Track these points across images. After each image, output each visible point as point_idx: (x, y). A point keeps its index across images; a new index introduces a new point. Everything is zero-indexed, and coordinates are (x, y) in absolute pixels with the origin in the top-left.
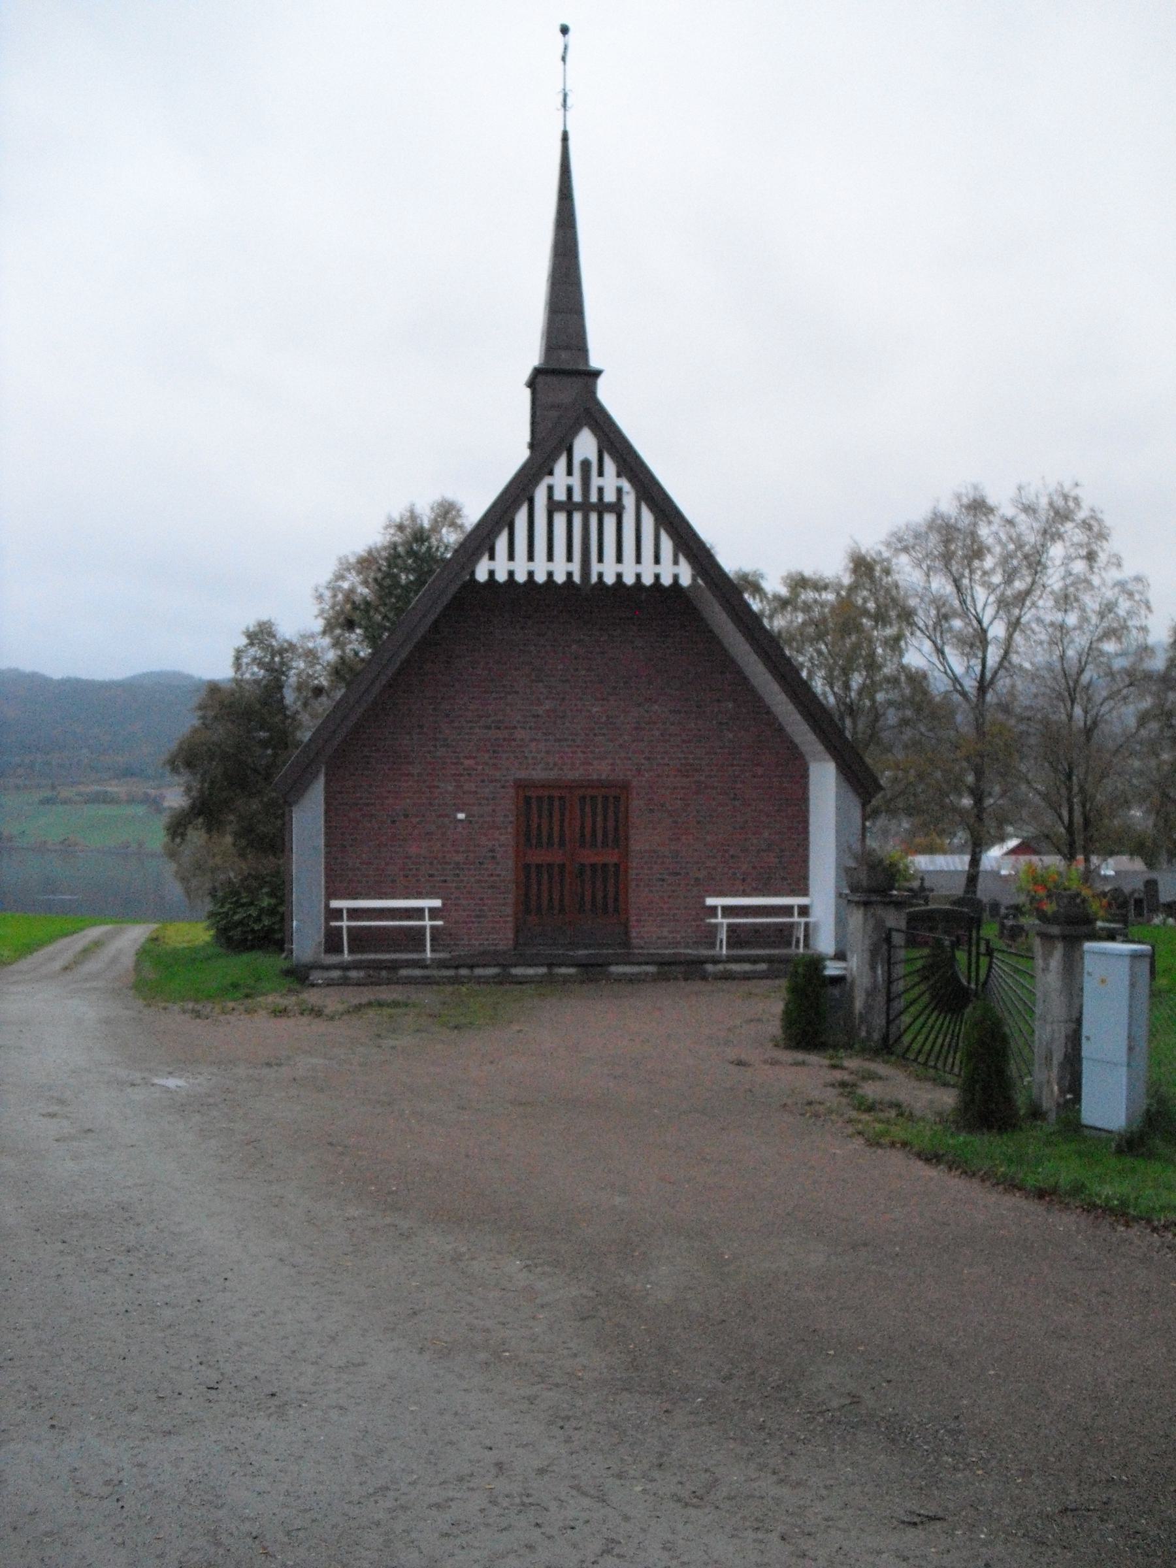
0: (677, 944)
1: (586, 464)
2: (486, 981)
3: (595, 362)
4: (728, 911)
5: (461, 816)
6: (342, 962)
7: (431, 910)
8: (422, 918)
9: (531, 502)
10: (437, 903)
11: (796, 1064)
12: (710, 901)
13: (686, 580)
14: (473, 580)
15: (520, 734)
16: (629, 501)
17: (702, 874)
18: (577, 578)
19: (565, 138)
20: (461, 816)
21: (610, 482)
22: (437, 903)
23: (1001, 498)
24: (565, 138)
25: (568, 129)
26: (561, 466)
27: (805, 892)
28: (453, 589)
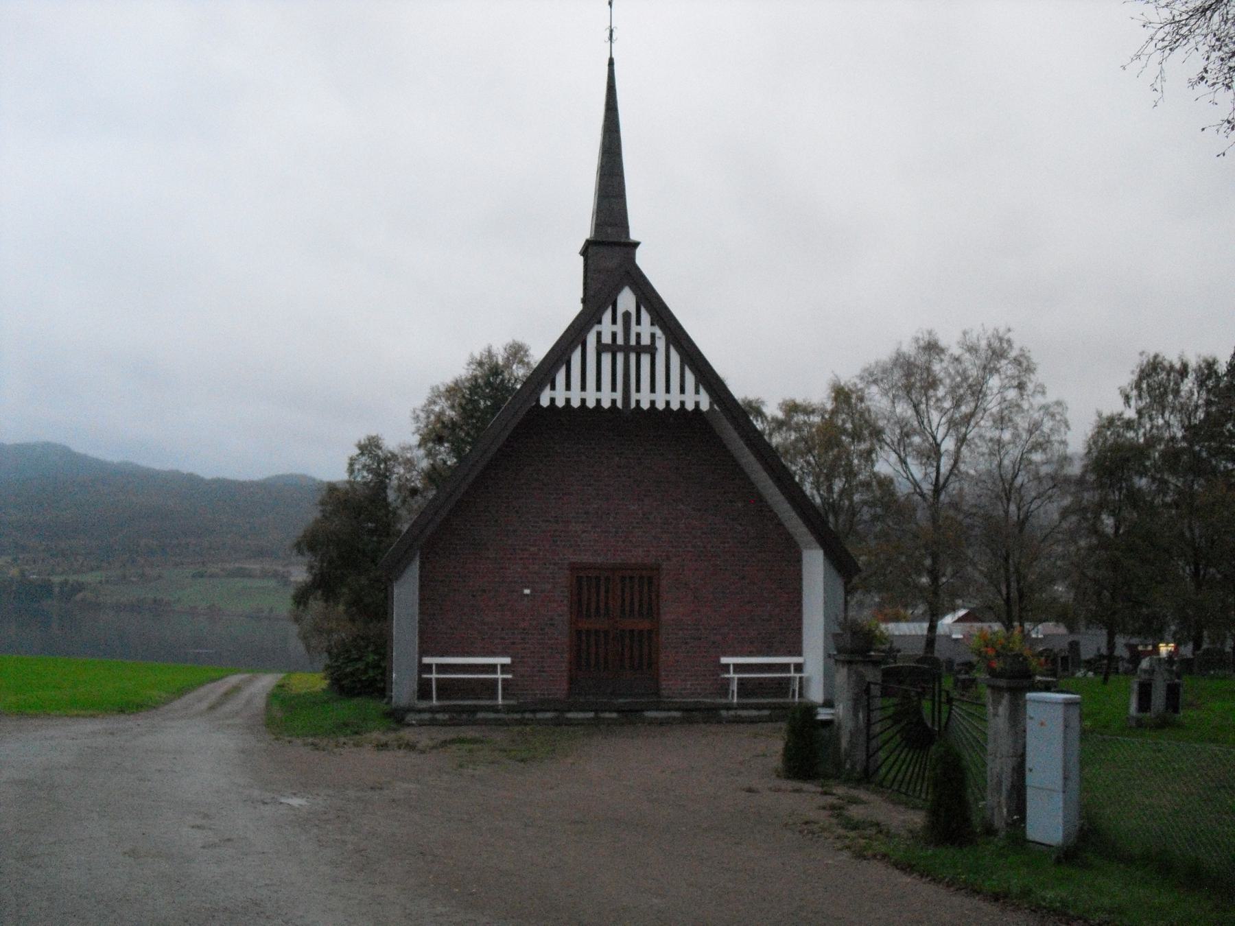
1: (627, 315)
4: (739, 668)
5: (527, 591)
7: (503, 666)
8: (495, 672)
10: (507, 660)
12: (724, 660)
14: (538, 405)
16: (661, 344)
18: (619, 404)
20: (527, 591)
21: (646, 329)
23: (950, 340)
26: (607, 316)
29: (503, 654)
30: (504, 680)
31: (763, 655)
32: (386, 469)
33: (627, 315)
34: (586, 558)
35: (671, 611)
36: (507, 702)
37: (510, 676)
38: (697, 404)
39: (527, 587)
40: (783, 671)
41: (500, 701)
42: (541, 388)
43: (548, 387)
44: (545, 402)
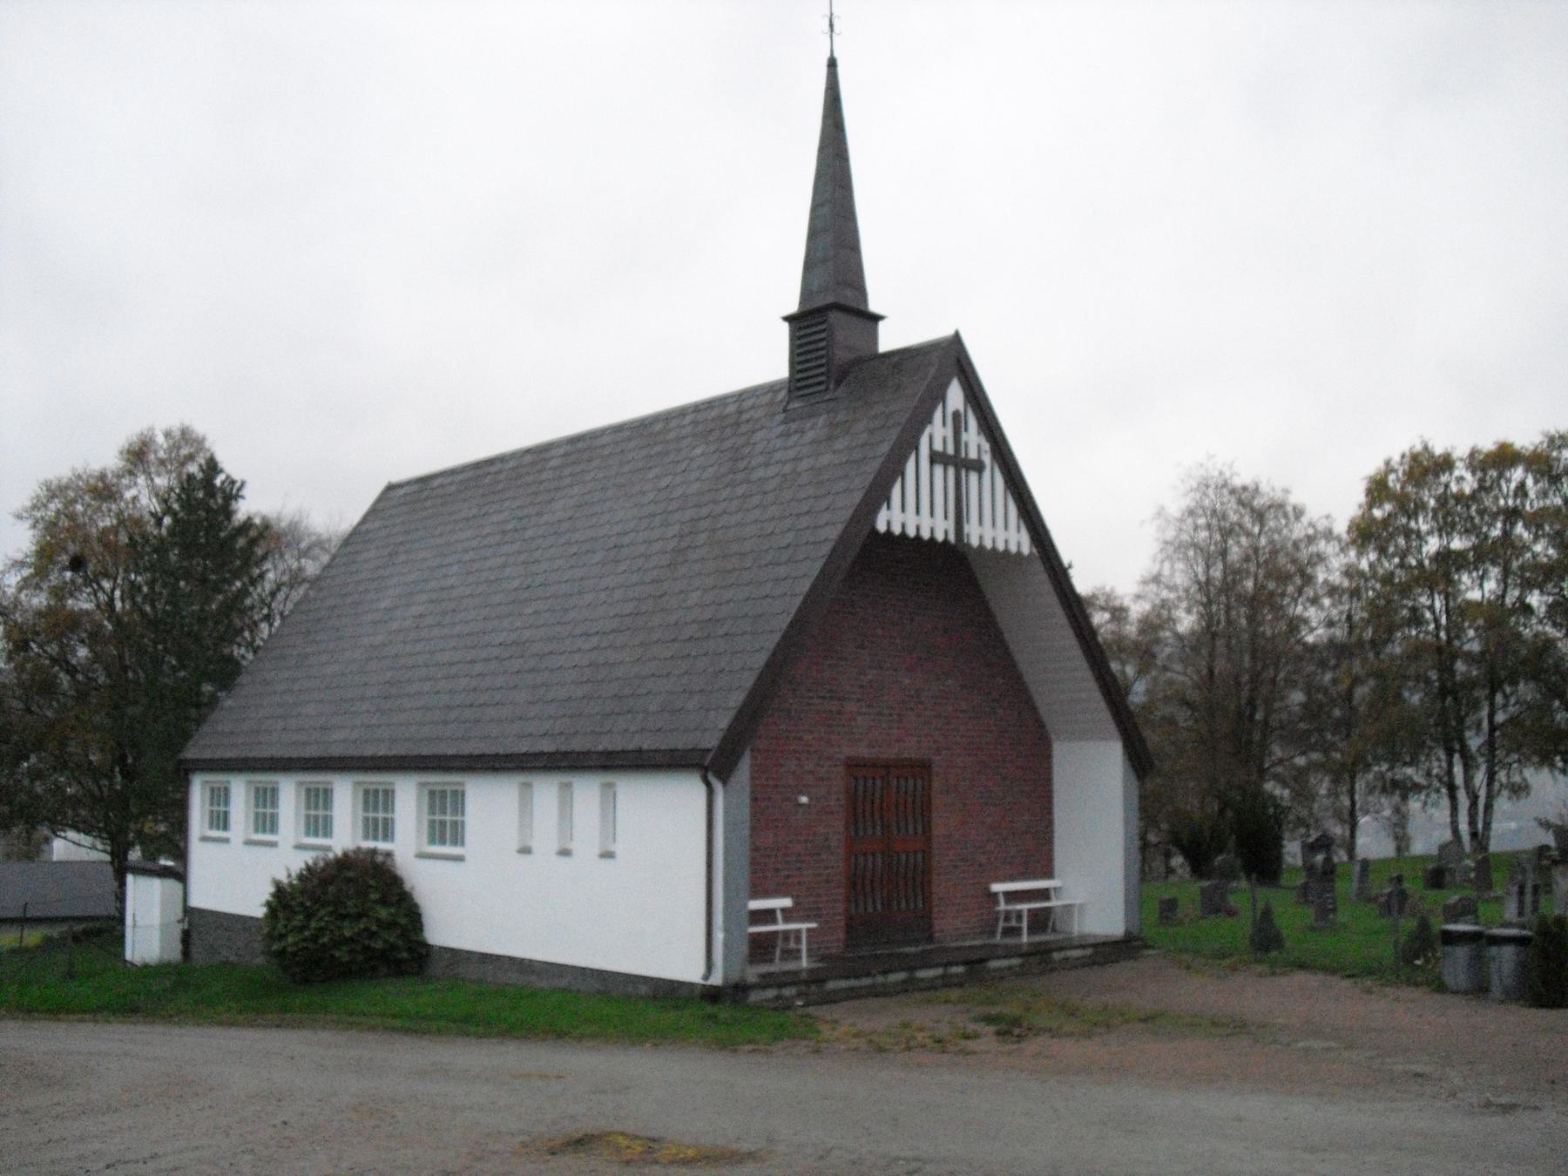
0: (964, 936)
1: (956, 415)
2: (931, 985)
3: (874, 306)
4: (1012, 896)
5: (804, 799)
6: (796, 973)
7: (783, 910)
8: (774, 921)
9: (917, 449)
10: (787, 902)
11: (1010, 1053)
12: (997, 887)
13: (1026, 550)
14: (874, 532)
15: (850, 707)
16: (987, 459)
17: (983, 859)
18: (952, 538)
19: (832, 64)
20: (804, 799)
21: (974, 442)
22: (787, 902)
23: (1264, 488)
24: (832, 64)
25: (836, 55)
26: (938, 415)
27: (1049, 874)
28: (859, 541)
29: (785, 895)
30: (809, 930)
31: (726, 908)
32: (1234, 581)
33: (956, 415)
34: (863, 751)
35: (944, 822)
36: (1037, 938)
37: (814, 925)
38: (1019, 545)
39: (801, 793)
40: (766, 923)
41: (1025, 938)
42: (875, 511)
43: (885, 506)
44: (881, 527)
